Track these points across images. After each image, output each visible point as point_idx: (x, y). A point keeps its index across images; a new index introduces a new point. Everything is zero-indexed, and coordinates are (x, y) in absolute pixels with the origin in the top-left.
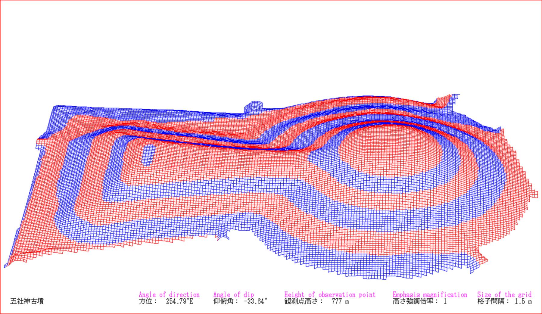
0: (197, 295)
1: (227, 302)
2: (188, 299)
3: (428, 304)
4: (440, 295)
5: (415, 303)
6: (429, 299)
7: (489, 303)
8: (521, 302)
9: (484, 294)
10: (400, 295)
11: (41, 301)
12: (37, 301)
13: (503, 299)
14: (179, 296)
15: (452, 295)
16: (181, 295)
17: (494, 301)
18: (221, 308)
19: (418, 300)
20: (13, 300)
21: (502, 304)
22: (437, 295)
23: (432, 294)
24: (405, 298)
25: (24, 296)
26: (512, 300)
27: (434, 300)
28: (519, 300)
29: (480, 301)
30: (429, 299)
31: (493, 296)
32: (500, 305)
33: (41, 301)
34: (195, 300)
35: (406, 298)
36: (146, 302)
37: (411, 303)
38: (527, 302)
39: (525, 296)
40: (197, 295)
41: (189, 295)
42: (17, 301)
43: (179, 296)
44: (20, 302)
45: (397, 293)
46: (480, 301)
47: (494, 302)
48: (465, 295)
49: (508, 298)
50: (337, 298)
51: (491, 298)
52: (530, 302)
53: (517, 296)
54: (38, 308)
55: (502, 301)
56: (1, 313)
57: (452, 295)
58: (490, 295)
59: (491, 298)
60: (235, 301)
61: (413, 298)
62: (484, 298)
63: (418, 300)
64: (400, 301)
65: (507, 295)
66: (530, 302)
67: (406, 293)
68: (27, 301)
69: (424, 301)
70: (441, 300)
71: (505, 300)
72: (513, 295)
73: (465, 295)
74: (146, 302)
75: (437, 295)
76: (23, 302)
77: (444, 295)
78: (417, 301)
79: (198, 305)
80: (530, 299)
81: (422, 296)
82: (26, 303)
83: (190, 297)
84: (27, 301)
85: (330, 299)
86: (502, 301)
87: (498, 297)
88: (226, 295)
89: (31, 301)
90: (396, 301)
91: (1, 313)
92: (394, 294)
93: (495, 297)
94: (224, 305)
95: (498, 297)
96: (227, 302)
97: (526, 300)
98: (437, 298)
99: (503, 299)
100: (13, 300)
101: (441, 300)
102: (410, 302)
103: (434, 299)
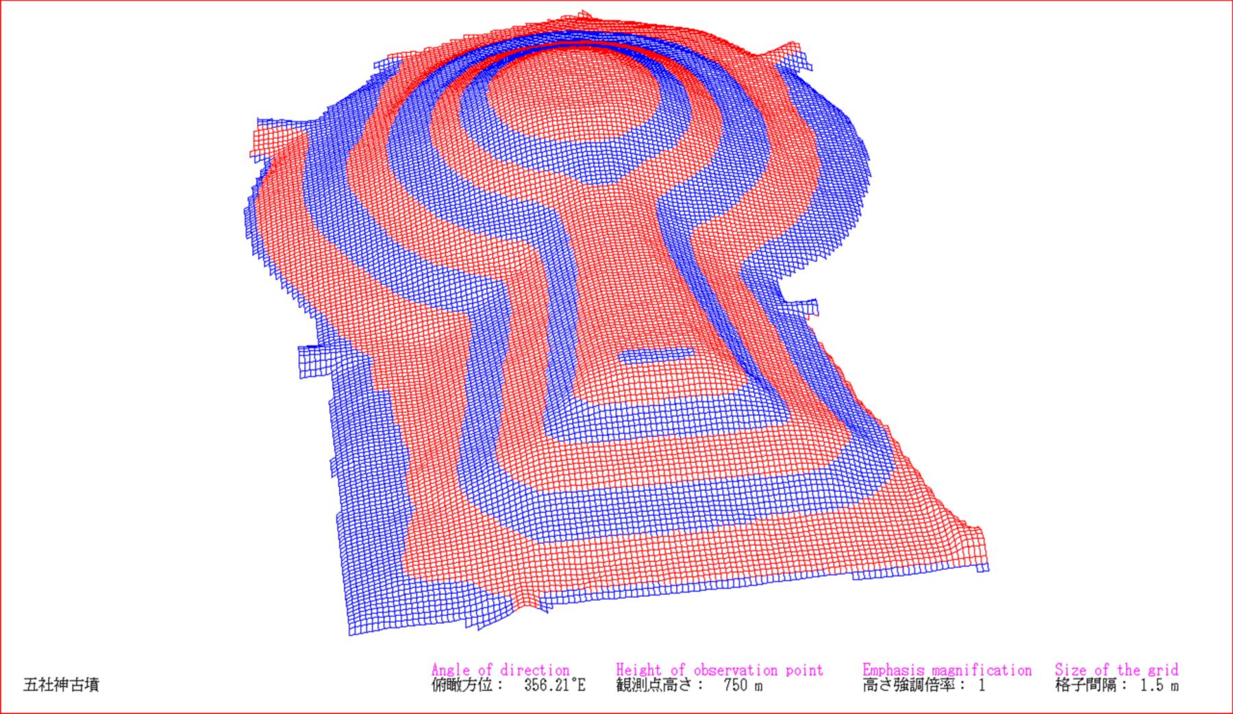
3: (942, 692)
4: (971, 672)
5: (913, 690)
7: (1083, 688)
8: (1155, 687)
9: (1070, 667)
10: (879, 671)
11: (94, 684)
12: (85, 684)
13: (1113, 680)
14: (522, 672)
15: (997, 672)
16: (527, 670)
17: (1093, 683)
18: (448, 699)
19: (920, 681)
20: (30, 681)
22: (964, 672)
24: (890, 678)
25: (54, 674)
26: (1134, 682)
27: (957, 682)
28: (1151, 682)
29: (1062, 685)
31: (1090, 674)
32: (1107, 694)
33: (94, 684)
35: (892, 679)
36: (477, 687)
37: (905, 688)
38: (1167, 687)
39: (1163, 673)
42: (38, 684)
43: (522, 672)
44: (46, 687)
45: (873, 666)
46: (1062, 685)
47: (1093, 687)
48: (1027, 671)
49: (1124, 678)
51: (1085, 678)
52: (1175, 687)
53: (1144, 673)
54: (86, 699)
55: (1111, 685)
56: (3, 711)
57: (997, 672)
59: (1085, 678)
61: (909, 677)
62: (1070, 677)
63: (920, 681)
64: (880, 684)
65: (1123, 670)
66: (1175, 687)
67: (892, 666)
68: (62, 684)
69: (934, 684)
70: (972, 682)
71: (1118, 683)
72: (1137, 670)
73: (1027, 671)
74: (477, 687)
75: (964, 672)
76: (52, 687)
77: (978, 671)
78: (918, 685)
80: (1174, 679)
81: (928, 674)
82: (60, 689)
84: (62, 684)
86: (1111, 685)
87: (1102, 676)
89: (70, 684)
90: (870, 684)
91: (3, 711)
92: (866, 669)
93: (1095, 676)
95: (1102, 676)
97: (1167, 681)
99: (1113, 680)
100: (30, 681)
101: (972, 682)
102: (903, 686)
103: (958, 680)
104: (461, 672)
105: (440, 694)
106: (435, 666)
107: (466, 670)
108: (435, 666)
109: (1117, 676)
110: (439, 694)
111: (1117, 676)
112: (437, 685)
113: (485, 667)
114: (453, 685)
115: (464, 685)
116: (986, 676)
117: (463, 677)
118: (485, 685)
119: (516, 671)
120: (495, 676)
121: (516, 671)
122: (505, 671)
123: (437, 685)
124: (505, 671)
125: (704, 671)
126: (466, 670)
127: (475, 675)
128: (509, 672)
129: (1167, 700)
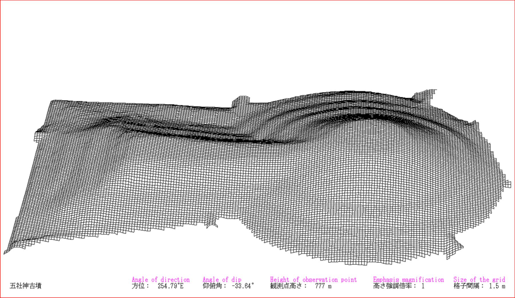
0: (188, 280)
1: (216, 286)
2: (179, 284)
3: (406, 289)
4: (418, 280)
5: (394, 288)
6: (407, 284)
7: (465, 287)
8: (495, 287)
9: (460, 279)
10: (380, 280)
11: (39, 286)
12: (35, 286)
13: (478, 284)
14: (170, 281)
15: (429, 280)
16: (172, 280)
17: (469, 285)
18: (210, 292)
19: (397, 284)
20: (13, 284)
21: (477, 289)
22: (415, 280)
23: (410, 279)
24: (384, 283)
25: (22, 281)
26: (487, 285)
27: (413, 284)
28: (493, 285)
29: (456, 286)
30: (407, 284)
31: (468, 281)
32: (475, 290)
33: (39, 286)
34: (185, 285)
35: (385, 283)
36: (138, 287)
37: (391, 287)
38: (500, 287)
39: (498, 281)
40: (188, 280)
41: (180, 280)
42: (16, 285)
43: (170, 281)
44: (19, 287)
45: (377, 278)
46: (456, 286)
47: (470, 287)
48: (442, 280)
49: (483, 283)
50: (320, 283)
51: (466, 283)
52: (504, 287)
53: (491, 281)
54: (36, 292)
55: (477, 286)
56: (1, 297)
57: (429, 280)
58: (465, 280)
59: (466, 283)
60: (223, 286)
61: (393, 283)
62: (460, 282)
63: (397, 284)
64: (380, 285)
65: (482, 280)
66: (504, 287)
67: (386, 278)
68: (26, 285)
69: (403, 286)
70: (419, 285)
71: (480, 285)
72: (488, 280)
73: (442, 280)
74: (138, 287)
75: (415, 280)
76: (22, 287)
77: (422, 280)
78: (396, 286)
79: (188, 289)
80: (503, 284)
81: (401, 281)
82: (25, 288)
83: (180, 282)
84: (26, 285)
85: (313, 284)
86: (477, 286)
87: (473, 282)
88: (215, 280)
89: (29, 285)
90: (376, 286)
91: (1, 297)
92: (374, 279)
93: (470, 282)
94: (213, 290)
95: (473, 282)
96: (216, 286)
97: (500, 284)
98: (415, 283)
99: (478, 284)
100: (13, 284)
101: (419, 285)
102: (390, 286)
103: (413, 284)
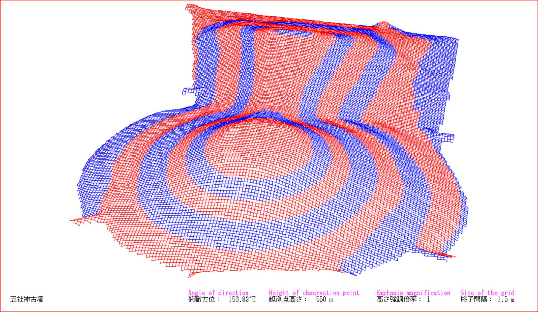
3: (411, 302)
4: (424, 293)
5: (398, 301)
7: (472, 301)
8: (504, 300)
9: (467, 292)
10: (384, 293)
11: (41, 299)
12: (37, 299)
13: (485, 297)
14: (228, 294)
15: (435, 294)
17: (477, 299)
18: (196, 305)
19: (401, 298)
20: (13, 298)
22: (421, 294)
24: (388, 296)
25: (23, 294)
26: (495, 298)
27: (418, 298)
28: (502, 298)
29: (463, 299)
31: (476, 294)
32: (483, 303)
33: (41, 299)
35: (389, 297)
36: (208, 300)
37: (395, 301)
38: (509, 300)
39: (507, 294)
42: (17, 299)
43: (228, 294)
44: (20, 300)
45: (381, 291)
46: (463, 299)
47: (477, 300)
48: (448, 293)
49: (491, 296)
51: (473, 296)
52: (513, 300)
53: (499, 294)
54: (37, 306)
55: (485, 299)
56: (1, 311)
57: (435, 294)
59: (473, 296)
61: (397, 296)
62: (467, 296)
63: (401, 298)
64: (384, 299)
65: (490, 293)
66: (513, 300)
67: (389, 291)
68: (27, 299)
69: (407, 299)
70: (424, 298)
71: (488, 298)
72: (496, 293)
73: (448, 293)
74: (208, 300)
75: (421, 294)
76: (23, 300)
77: (427, 293)
78: (401, 299)
80: (512, 297)
81: (405, 295)
82: (26, 301)
84: (27, 299)
85: (227, 298)
86: (485, 299)
87: (481, 296)
89: (31, 299)
90: (380, 299)
91: (1, 311)
92: (378, 292)
93: (478, 296)
95: (481, 296)
97: (509, 298)
99: (485, 297)
100: (13, 298)
101: (424, 298)
102: (394, 300)
103: (418, 297)
104: (201, 294)
105: (192, 303)
106: (190, 291)
107: (203, 293)
108: (190, 291)
109: (487, 295)
110: (192, 303)
111: (487, 295)
112: (191, 299)
113: (212, 291)
114: (198, 299)
115: (202, 299)
116: (430, 296)
117: (202, 296)
118: (211, 299)
119: (225, 293)
120: (216, 295)
121: (225, 293)
122: (220, 293)
123: (191, 299)
124: (220, 293)
125: (307, 293)
126: (203, 293)
127: (207, 295)
128: (222, 293)
129: (509, 306)
